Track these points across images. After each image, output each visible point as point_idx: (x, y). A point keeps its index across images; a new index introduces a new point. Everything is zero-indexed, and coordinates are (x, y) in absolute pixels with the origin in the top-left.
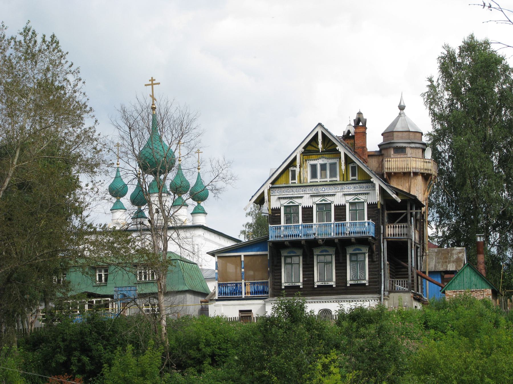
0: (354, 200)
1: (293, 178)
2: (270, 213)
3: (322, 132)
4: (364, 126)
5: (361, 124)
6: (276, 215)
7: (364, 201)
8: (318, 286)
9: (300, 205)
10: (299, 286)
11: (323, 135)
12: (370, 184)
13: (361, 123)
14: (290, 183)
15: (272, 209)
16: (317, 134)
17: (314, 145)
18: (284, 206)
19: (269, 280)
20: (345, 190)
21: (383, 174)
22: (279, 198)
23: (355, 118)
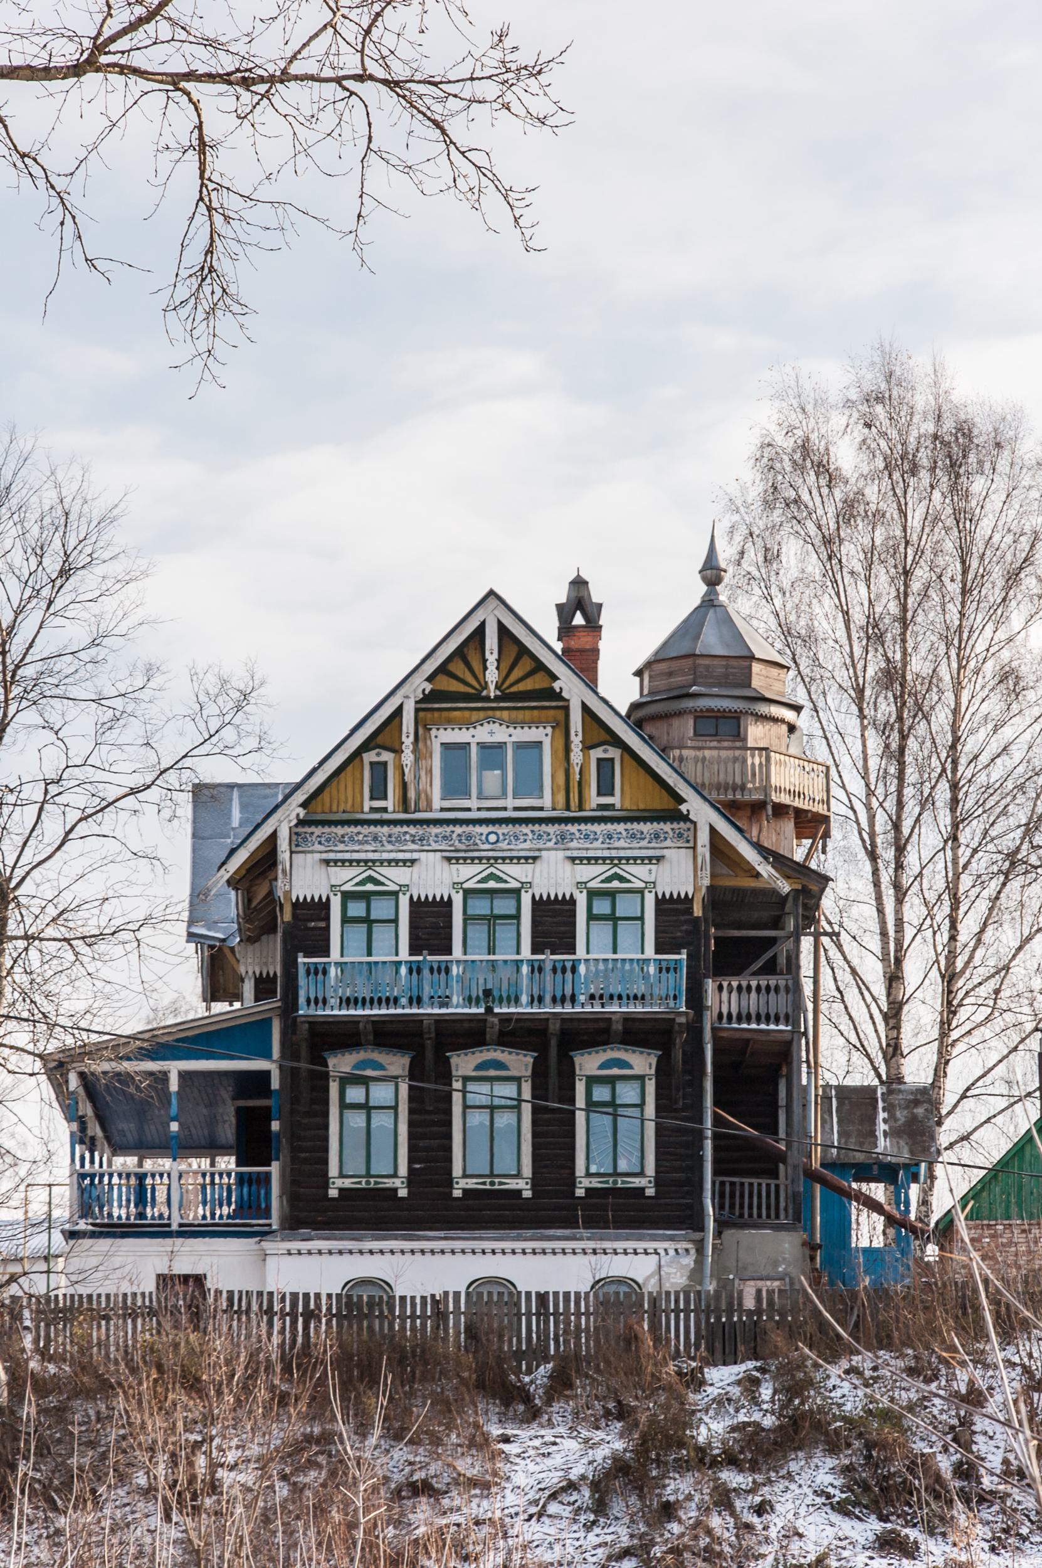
0: (608, 880)
1: (379, 792)
4: (593, 626)
8: (465, 1191)
10: (395, 1190)
14: (366, 809)
17: (460, 674)
19: (275, 1169)
20: (574, 844)
23: (564, 600)
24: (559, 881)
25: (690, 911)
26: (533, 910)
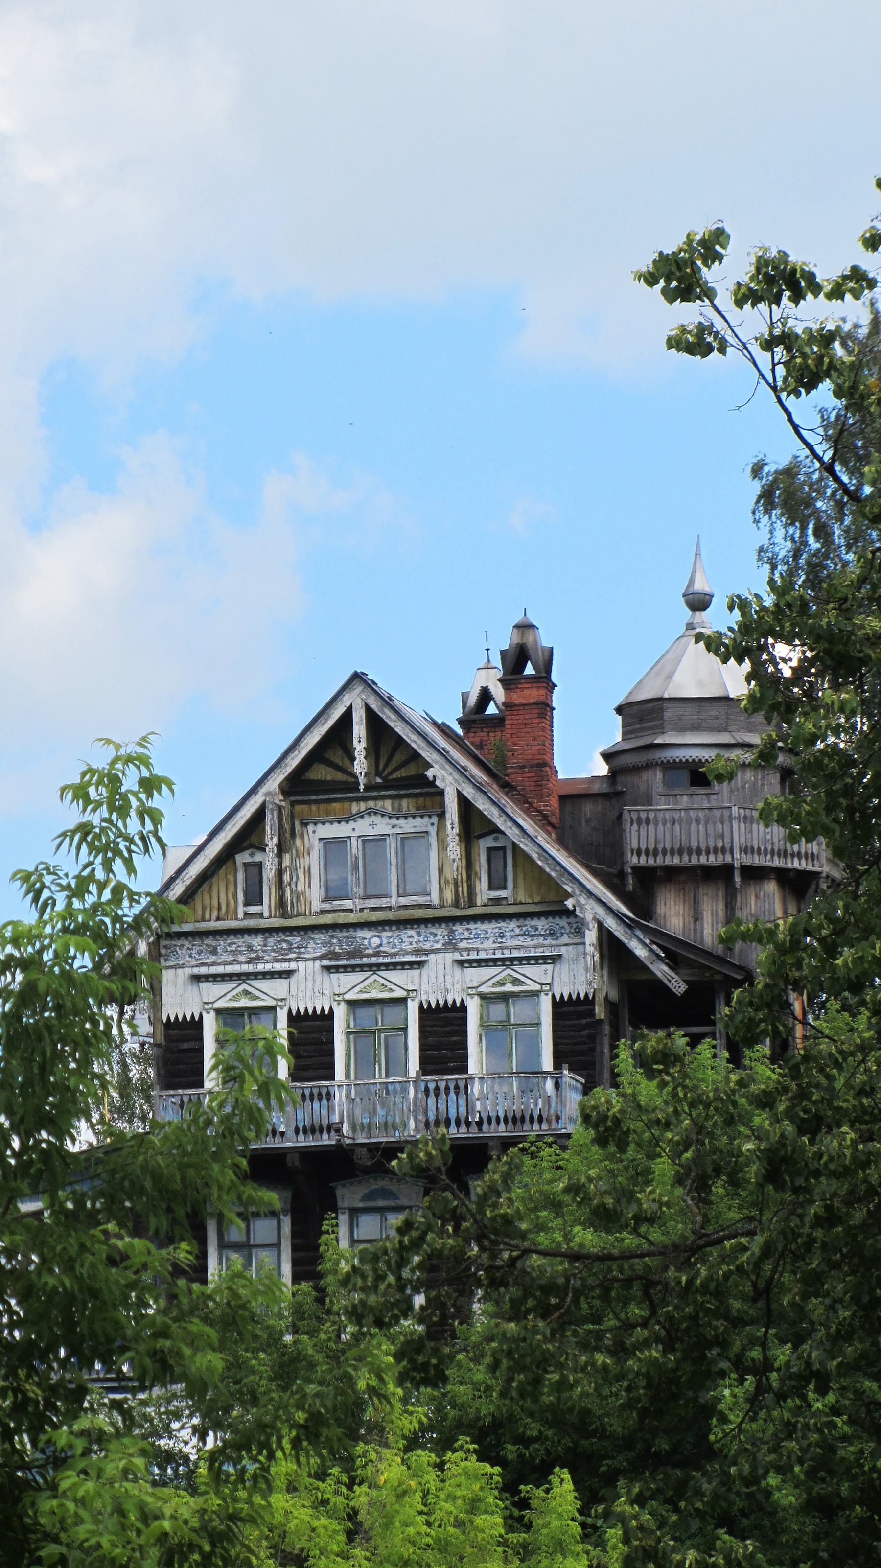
1: (254, 896)
2: (161, 1039)
3: (369, 711)
4: (544, 679)
5: (529, 670)
6: (49, 1054)
7: (538, 987)
9: (282, 1007)
11: (374, 721)
12: (563, 922)
13: (529, 664)
14: (241, 915)
15: (168, 1025)
16: (347, 716)
18: (219, 1012)
21: (622, 875)
22: (197, 979)
23: (506, 647)
24: (449, 986)
25: (592, 1013)
26: (421, 1019)
